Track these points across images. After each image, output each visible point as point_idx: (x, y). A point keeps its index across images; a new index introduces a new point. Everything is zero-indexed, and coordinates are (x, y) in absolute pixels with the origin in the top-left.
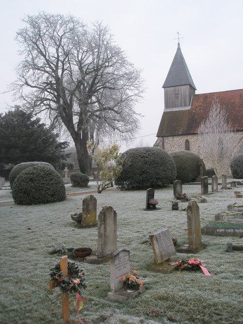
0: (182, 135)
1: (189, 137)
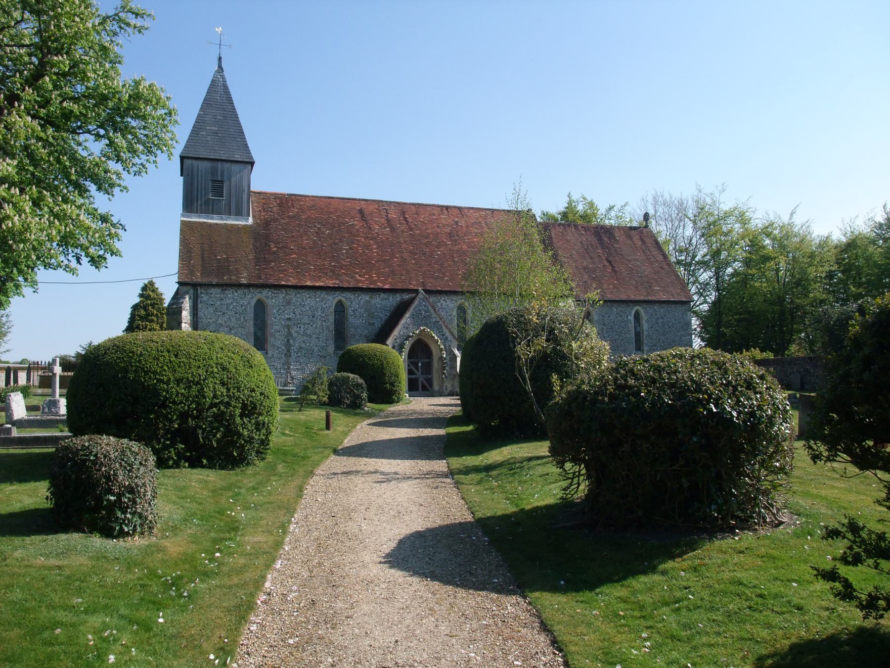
0: (248, 286)
1: (265, 294)
